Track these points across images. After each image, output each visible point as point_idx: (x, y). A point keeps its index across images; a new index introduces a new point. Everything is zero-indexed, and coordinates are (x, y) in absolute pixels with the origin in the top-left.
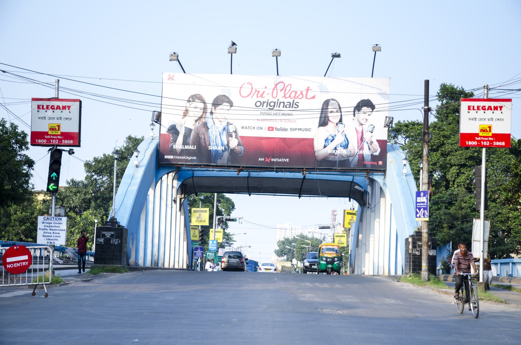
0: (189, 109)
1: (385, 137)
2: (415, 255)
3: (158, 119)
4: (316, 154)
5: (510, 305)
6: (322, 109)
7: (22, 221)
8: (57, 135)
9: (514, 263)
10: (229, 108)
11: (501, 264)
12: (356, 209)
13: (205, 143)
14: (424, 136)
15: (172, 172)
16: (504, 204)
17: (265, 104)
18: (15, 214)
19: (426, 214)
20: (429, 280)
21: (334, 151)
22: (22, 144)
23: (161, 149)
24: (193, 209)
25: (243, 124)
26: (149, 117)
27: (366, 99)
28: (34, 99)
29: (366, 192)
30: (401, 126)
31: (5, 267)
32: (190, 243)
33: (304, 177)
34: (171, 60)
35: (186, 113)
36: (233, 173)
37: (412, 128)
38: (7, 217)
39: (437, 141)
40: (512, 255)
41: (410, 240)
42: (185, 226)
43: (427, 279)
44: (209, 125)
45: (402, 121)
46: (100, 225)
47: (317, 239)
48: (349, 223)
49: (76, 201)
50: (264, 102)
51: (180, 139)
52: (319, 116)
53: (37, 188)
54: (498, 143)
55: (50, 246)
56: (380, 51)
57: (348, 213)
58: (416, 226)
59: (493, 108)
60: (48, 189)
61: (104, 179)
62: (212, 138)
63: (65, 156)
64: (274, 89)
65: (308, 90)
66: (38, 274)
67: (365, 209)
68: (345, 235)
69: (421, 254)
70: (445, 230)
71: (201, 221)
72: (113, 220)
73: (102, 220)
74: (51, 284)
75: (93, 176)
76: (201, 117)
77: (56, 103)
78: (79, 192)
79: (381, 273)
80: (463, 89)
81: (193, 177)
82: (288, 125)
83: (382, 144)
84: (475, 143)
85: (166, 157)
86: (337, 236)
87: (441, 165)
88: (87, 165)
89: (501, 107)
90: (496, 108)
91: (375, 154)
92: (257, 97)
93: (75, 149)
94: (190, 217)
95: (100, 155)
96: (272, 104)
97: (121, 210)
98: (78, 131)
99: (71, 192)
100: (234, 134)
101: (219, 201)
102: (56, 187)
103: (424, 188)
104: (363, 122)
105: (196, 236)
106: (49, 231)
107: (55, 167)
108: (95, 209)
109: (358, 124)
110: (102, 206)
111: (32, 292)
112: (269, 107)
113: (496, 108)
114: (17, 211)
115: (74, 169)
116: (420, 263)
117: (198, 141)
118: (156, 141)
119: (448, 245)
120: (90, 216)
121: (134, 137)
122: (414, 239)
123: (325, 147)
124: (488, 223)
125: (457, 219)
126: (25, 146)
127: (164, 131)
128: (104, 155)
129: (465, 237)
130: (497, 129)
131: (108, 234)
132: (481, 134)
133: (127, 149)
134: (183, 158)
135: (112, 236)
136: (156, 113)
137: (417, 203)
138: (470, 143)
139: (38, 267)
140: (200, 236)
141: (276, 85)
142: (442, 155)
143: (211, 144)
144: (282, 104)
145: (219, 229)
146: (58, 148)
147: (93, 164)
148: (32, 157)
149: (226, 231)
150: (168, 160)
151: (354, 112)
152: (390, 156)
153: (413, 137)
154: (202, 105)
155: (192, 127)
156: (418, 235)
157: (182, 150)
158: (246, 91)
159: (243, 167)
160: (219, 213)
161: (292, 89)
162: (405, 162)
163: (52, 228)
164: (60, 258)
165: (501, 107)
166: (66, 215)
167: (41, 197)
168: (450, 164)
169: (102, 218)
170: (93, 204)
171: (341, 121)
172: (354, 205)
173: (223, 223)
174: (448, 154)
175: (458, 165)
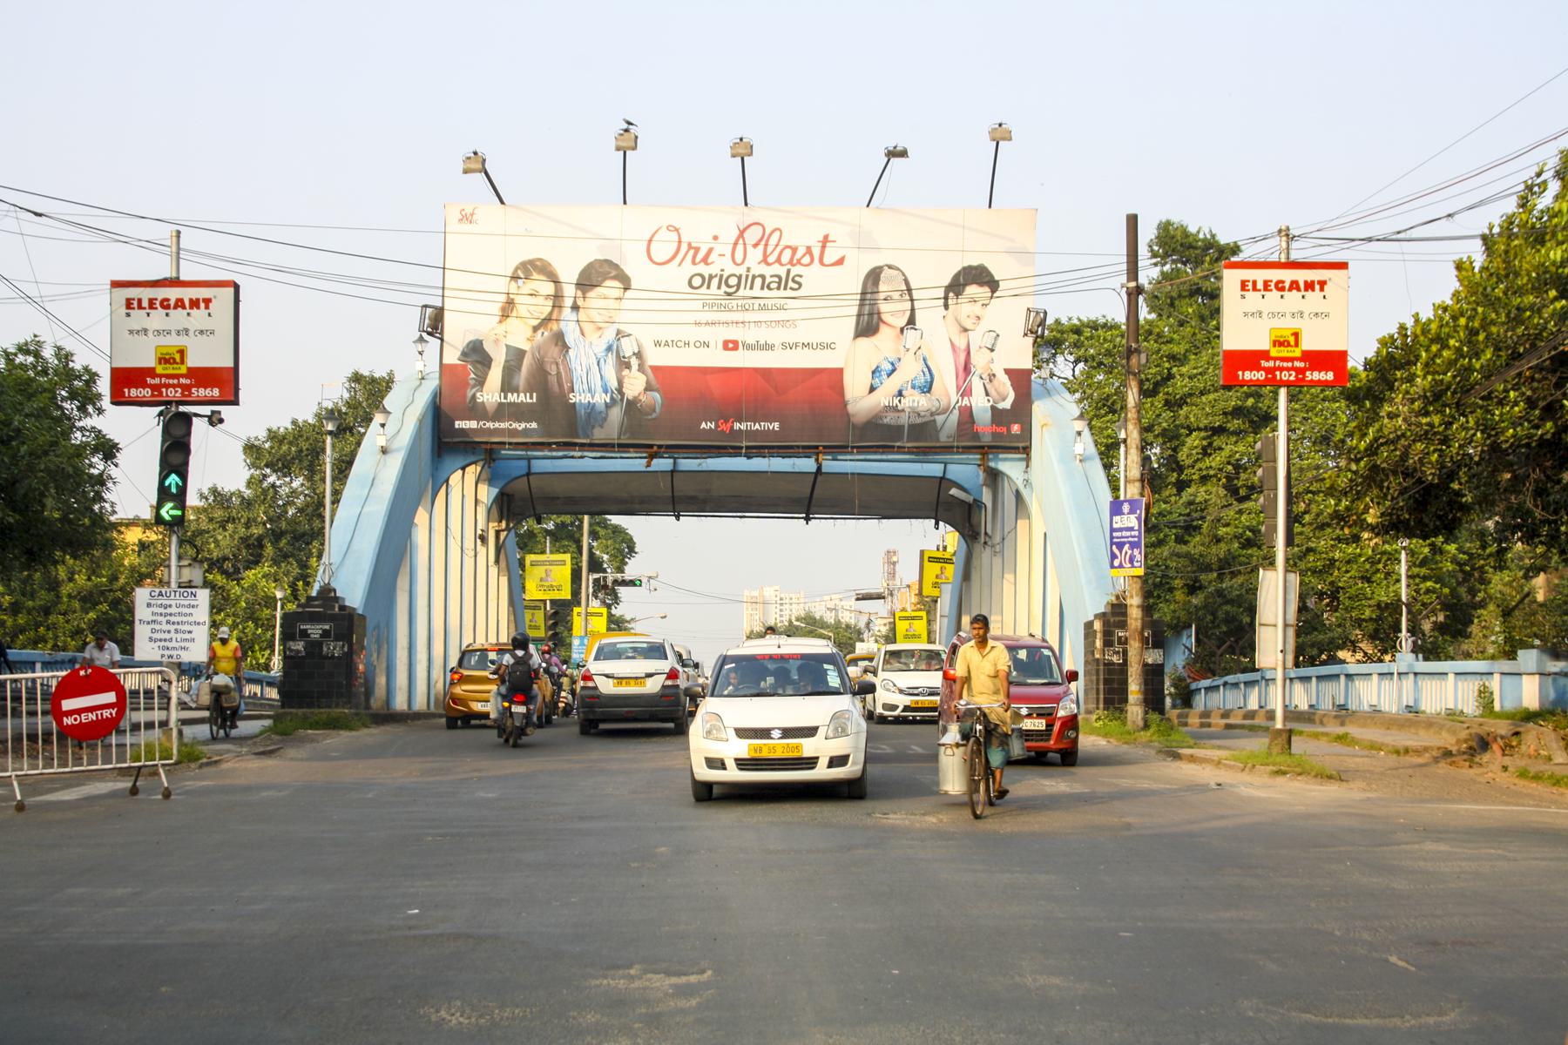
0: (518, 299)
1: (1026, 363)
2: (1111, 664)
3: (435, 324)
4: (850, 408)
5: (1351, 785)
6: (863, 293)
7: (89, 599)
8: (177, 377)
9: (1349, 676)
10: (619, 293)
11: (1319, 678)
12: (950, 550)
13: (560, 385)
14: (1128, 358)
15: (475, 463)
16: (1322, 527)
17: (715, 282)
18: (71, 580)
19: (1138, 557)
20: (1146, 726)
21: (896, 401)
22: (86, 398)
23: (445, 407)
24: (530, 558)
25: (656, 332)
26: (411, 322)
27: (975, 263)
28: (116, 284)
29: (978, 504)
30: (1062, 332)
31: (60, 723)
33: (819, 468)
34: (465, 172)
36: (636, 463)
37: (1092, 338)
38: (49, 590)
39: (1153, 371)
40: (1341, 654)
41: (1097, 626)
43: (1141, 723)
44: (569, 340)
45: (1064, 320)
46: (292, 607)
47: (848, 626)
48: (936, 585)
49: (223, 542)
50: (711, 277)
51: (495, 376)
52: (855, 310)
53: (123, 513)
54: (1317, 376)
55: (170, 665)
56: (1010, 139)
57: (931, 559)
58: (1111, 590)
59: (1302, 286)
60: (159, 520)
61: (295, 484)
62: (578, 373)
63: (199, 427)
64: (736, 244)
66: (143, 737)
67: (978, 547)
68: (923, 614)
69: (1125, 661)
70: (1179, 595)
72: (328, 594)
74: (176, 763)
75: (265, 476)
76: (547, 320)
77: (173, 294)
80: (1213, 236)
81: (528, 474)
82: (775, 336)
83: (1020, 379)
85: (458, 424)
86: (902, 618)
87: (1165, 430)
88: (251, 449)
89: (1322, 284)
90: (1309, 286)
91: (1001, 406)
92: (694, 263)
93: (225, 411)
94: (522, 577)
95: (283, 424)
96: (733, 281)
97: (346, 564)
98: (231, 365)
99: (211, 520)
100: (634, 362)
101: (594, 535)
102: (179, 513)
103: (1131, 491)
104: (968, 324)
105: (537, 628)
106: (165, 627)
107: (175, 459)
109: (955, 329)
110: (293, 555)
111: (130, 785)
112: (723, 287)
113: (1309, 286)
114: (73, 573)
115: (220, 463)
116: (1124, 683)
117: (541, 380)
118: (432, 384)
119: (1185, 633)
120: (264, 583)
121: (366, 373)
122: (1106, 624)
123: (872, 389)
124: (1294, 579)
125: (1207, 568)
126: (94, 405)
127: (452, 357)
128: (294, 422)
129: (1227, 613)
130: (1314, 341)
131: (315, 631)
133: (353, 404)
134: (504, 425)
135: (325, 634)
136: (429, 311)
137: (1112, 530)
138: (1248, 375)
139: (142, 717)
140: (548, 628)
141: (742, 233)
142: (1168, 404)
143: (576, 388)
144: (758, 281)
145: (595, 605)
146: (182, 409)
147: (267, 445)
148: (112, 433)
149: (614, 611)
151: (946, 298)
152: (1040, 410)
153: (1093, 358)
154: (549, 288)
155: (526, 346)
156: (1115, 614)
157: (501, 404)
158: (662, 250)
159: (660, 447)
160: (595, 566)
161: (783, 243)
162: (1081, 425)
163: (173, 619)
165: (1322, 284)
166: (206, 584)
167: (133, 536)
168: (1188, 427)
169: (293, 586)
170: (269, 550)
171: (911, 321)
172: (949, 538)
173: (608, 592)
174: (1182, 402)
175: (1206, 429)
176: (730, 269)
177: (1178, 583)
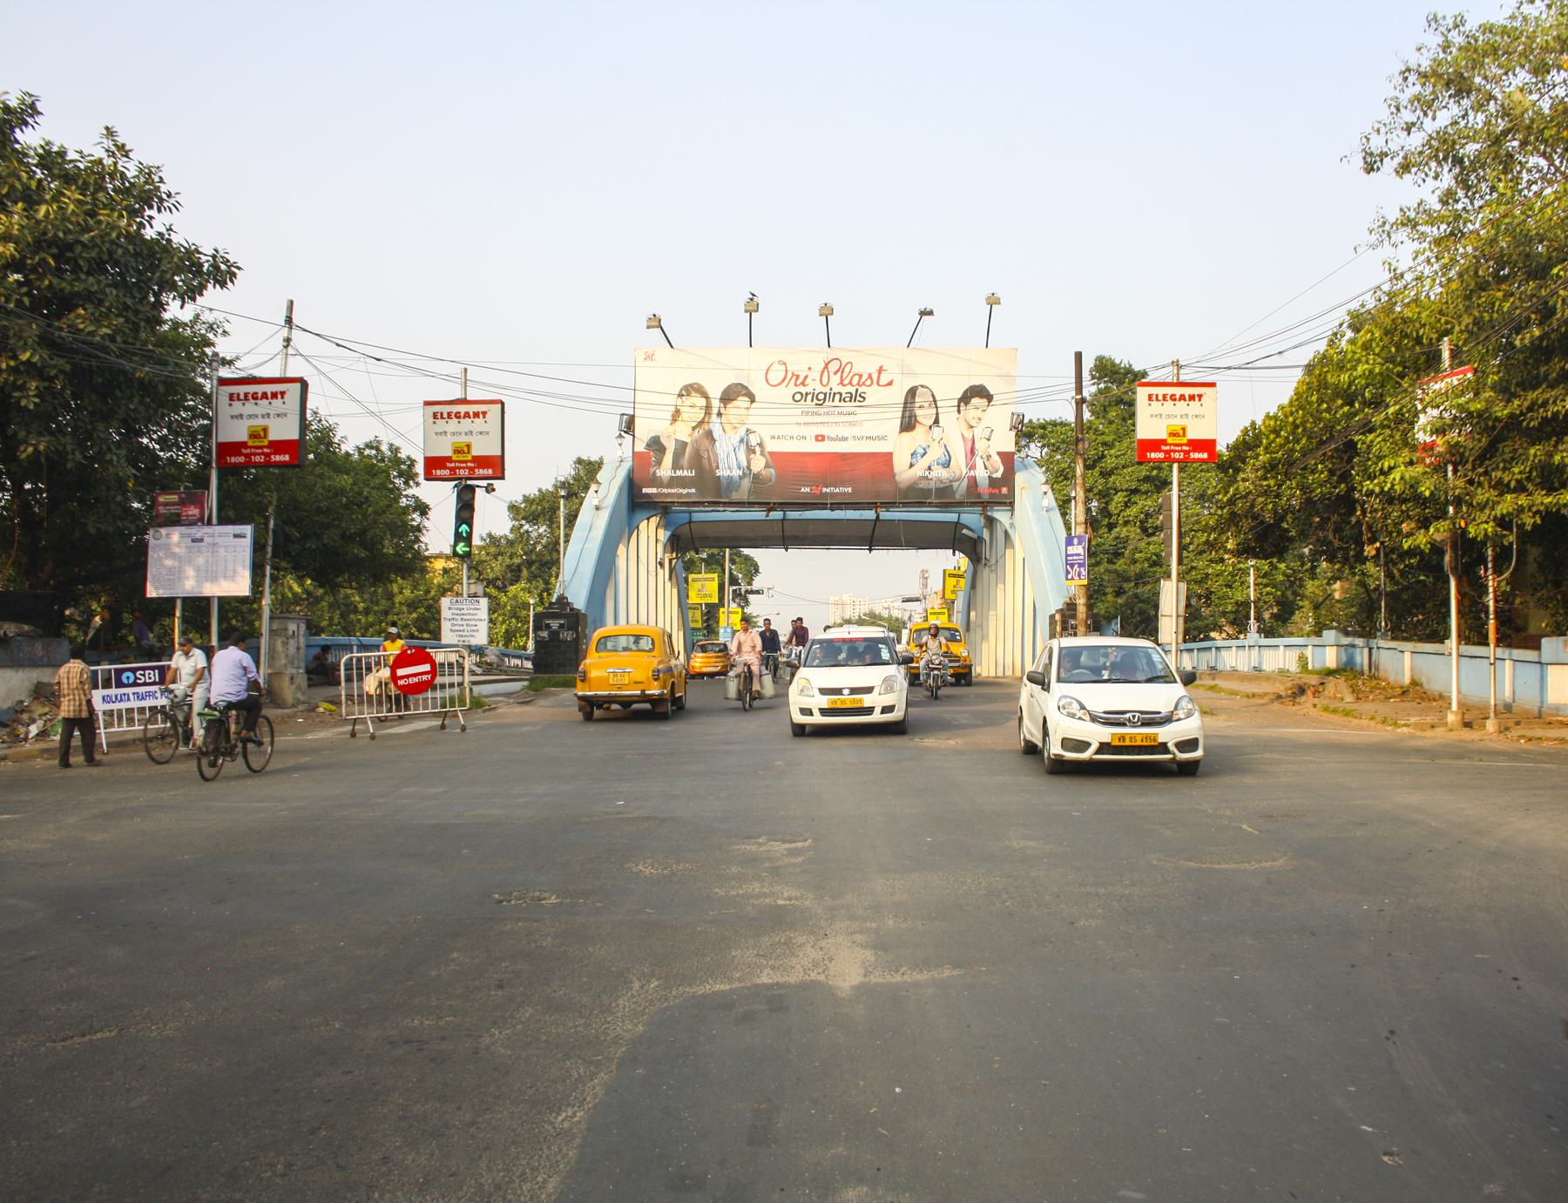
3: (629, 426)
7: (412, 605)
10: (747, 404)
16: (1201, 553)
22: (409, 476)
23: (636, 478)
24: (691, 576)
25: (772, 431)
28: (427, 403)
29: (980, 539)
32: (689, 632)
35: (676, 415)
36: (759, 515)
40: (1213, 634)
41: (1058, 617)
42: (680, 605)
44: (716, 435)
46: (540, 609)
49: (496, 568)
51: (668, 459)
53: (433, 550)
60: (455, 554)
62: (722, 456)
63: (480, 494)
65: (880, 370)
67: (980, 567)
70: (1110, 598)
71: (706, 596)
72: (562, 600)
73: (541, 599)
76: (702, 422)
77: (463, 409)
78: (501, 554)
79: (1009, 673)
83: (1007, 458)
84: (1161, 455)
85: (644, 490)
88: (513, 508)
89: (1200, 396)
90: (1192, 398)
93: (496, 483)
95: (533, 492)
97: (574, 579)
101: (733, 561)
103: (1079, 530)
107: (465, 515)
108: (529, 581)
113: (1192, 398)
117: (698, 461)
118: (628, 464)
122: (1063, 616)
123: (911, 466)
124: (1183, 586)
125: (1128, 580)
127: (640, 447)
131: (555, 624)
132: (1170, 441)
133: (577, 478)
135: (562, 626)
139: (447, 680)
142: (1102, 474)
145: (734, 606)
150: (647, 495)
152: (1020, 478)
154: (703, 402)
155: (688, 440)
156: (1071, 607)
158: (776, 376)
160: (734, 581)
164: (477, 665)
165: (1200, 396)
166: (486, 595)
167: (439, 565)
169: (540, 595)
170: (525, 573)
171: (936, 421)
172: (961, 561)
173: (742, 598)
174: (1111, 473)
176: (819, 389)
177: (1109, 590)
